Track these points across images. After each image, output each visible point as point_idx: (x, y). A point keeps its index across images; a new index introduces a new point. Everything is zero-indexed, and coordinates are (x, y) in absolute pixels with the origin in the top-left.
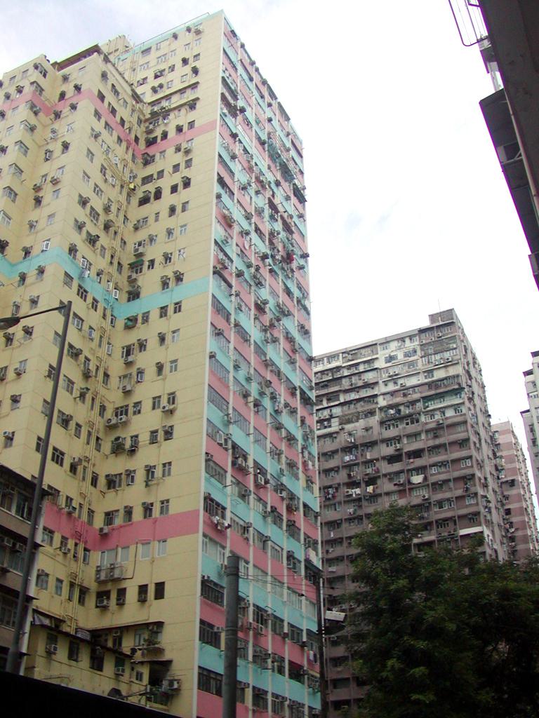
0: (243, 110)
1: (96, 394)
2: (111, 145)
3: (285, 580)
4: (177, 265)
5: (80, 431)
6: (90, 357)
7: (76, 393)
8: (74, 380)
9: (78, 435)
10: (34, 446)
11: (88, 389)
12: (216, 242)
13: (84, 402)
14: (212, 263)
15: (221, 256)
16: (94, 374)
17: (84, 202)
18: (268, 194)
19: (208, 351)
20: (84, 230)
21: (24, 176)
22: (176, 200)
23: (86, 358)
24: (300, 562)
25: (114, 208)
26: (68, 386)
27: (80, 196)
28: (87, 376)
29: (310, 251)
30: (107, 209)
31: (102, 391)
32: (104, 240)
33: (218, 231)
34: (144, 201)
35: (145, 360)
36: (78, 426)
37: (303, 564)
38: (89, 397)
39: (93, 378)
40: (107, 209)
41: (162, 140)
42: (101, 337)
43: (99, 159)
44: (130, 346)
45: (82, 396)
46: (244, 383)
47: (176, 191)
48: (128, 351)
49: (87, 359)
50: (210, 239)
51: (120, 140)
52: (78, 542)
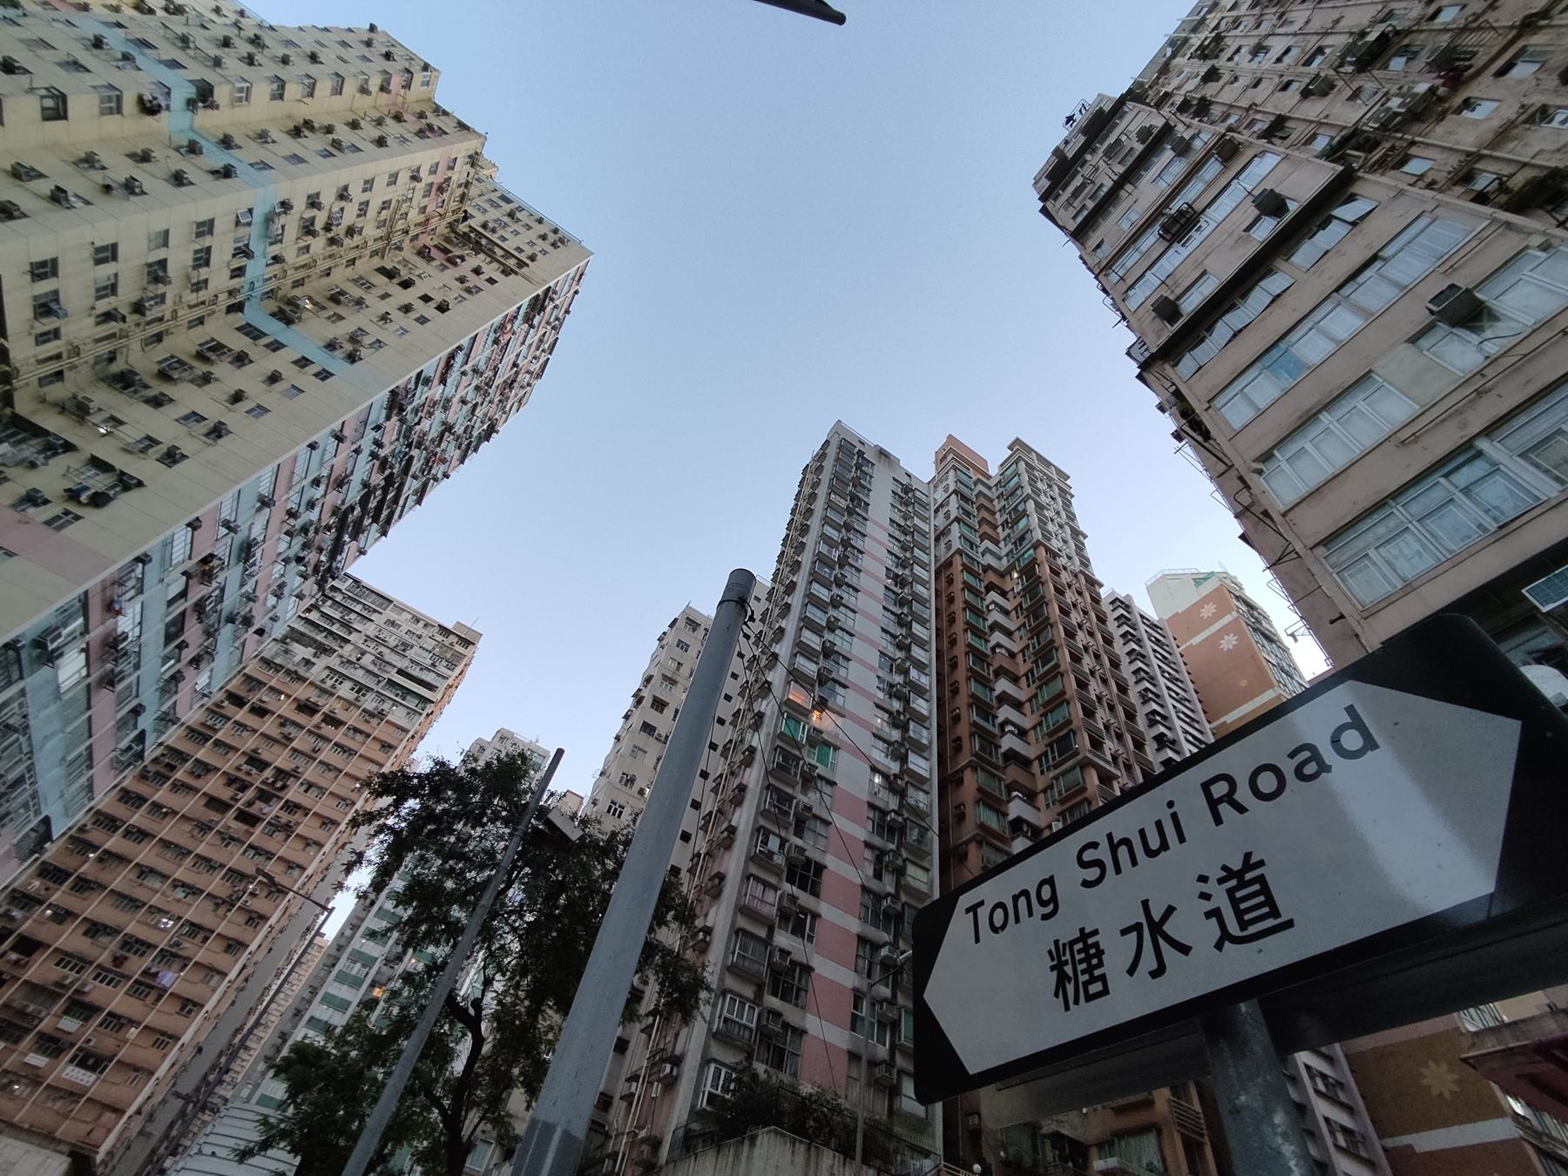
0: (531, 326)
1: (124, 335)
2: (414, 203)
3: (82, 748)
4: (234, 418)
5: (49, 341)
6: (169, 299)
7: (103, 305)
8: (120, 291)
9: (43, 338)
10: (38, 258)
11: (124, 319)
12: (419, 374)
13: (98, 324)
14: (401, 382)
15: (412, 386)
16: (149, 318)
17: (343, 195)
18: (479, 400)
19: (314, 438)
20: (314, 212)
21: (307, 100)
22: (291, 374)
23: (163, 296)
24: (135, 727)
25: (357, 240)
26: (105, 288)
27: (318, 195)
28: (138, 308)
29: (370, 552)
30: (351, 231)
31: (135, 345)
32: (318, 244)
33: (430, 367)
34: (390, 274)
35: (228, 376)
36: (307, 248)
37: (136, 732)
38: (113, 327)
39: (143, 320)
40: (351, 231)
41: (267, 346)
42: (203, 303)
43: (394, 194)
44: (224, 346)
45: (108, 317)
46: (323, 487)
47: (303, 367)
48: (218, 348)
49: (162, 299)
50: (546, 282)
51: (423, 210)
52: (65, 356)
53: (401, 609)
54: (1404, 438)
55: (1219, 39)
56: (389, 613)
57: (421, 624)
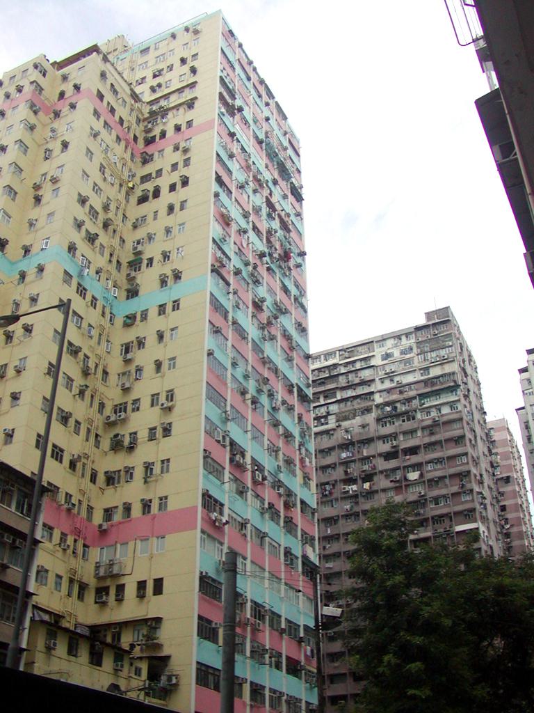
0: (240, 110)
1: (95, 391)
2: (110, 144)
5: (79, 428)
6: (89, 354)
7: (76, 390)
8: (73, 377)
9: (77, 432)
10: (34, 442)
11: (87, 387)
12: (214, 241)
13: (83, 400)
14: (210, 261)
15: (219, 254)
16: (93, 371)
17: (83, 201)
18: (266, 192)
19: (206, 349)
20: (84, 228)
21: (24, 175)
23: (85, 355)
24: (297, 558)
25: (113, 207)
26: (68, 383)
27: (80, 195)
28: (86, 373)
30: (106, 208)
31: (101, 388)
32: (103, 239)
33: (216, 230)
34: (143, 199)
35: (144, 358)
36: (78, 423)
37: (300, 560)
38: (88, 394)
39: (92, 376)
40: (106, 208)
42: (100, 335)
43: (98, 158)
44: (129, 343)
45: (82, 393)
48: (127, 348)
49: (86, 357)
51: (118, 139)
53: (382, 340)
54: (218, 554)
55: (138, 254)
56: (378, 352)
57: (404, 338)
